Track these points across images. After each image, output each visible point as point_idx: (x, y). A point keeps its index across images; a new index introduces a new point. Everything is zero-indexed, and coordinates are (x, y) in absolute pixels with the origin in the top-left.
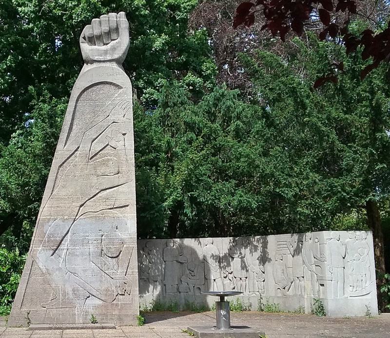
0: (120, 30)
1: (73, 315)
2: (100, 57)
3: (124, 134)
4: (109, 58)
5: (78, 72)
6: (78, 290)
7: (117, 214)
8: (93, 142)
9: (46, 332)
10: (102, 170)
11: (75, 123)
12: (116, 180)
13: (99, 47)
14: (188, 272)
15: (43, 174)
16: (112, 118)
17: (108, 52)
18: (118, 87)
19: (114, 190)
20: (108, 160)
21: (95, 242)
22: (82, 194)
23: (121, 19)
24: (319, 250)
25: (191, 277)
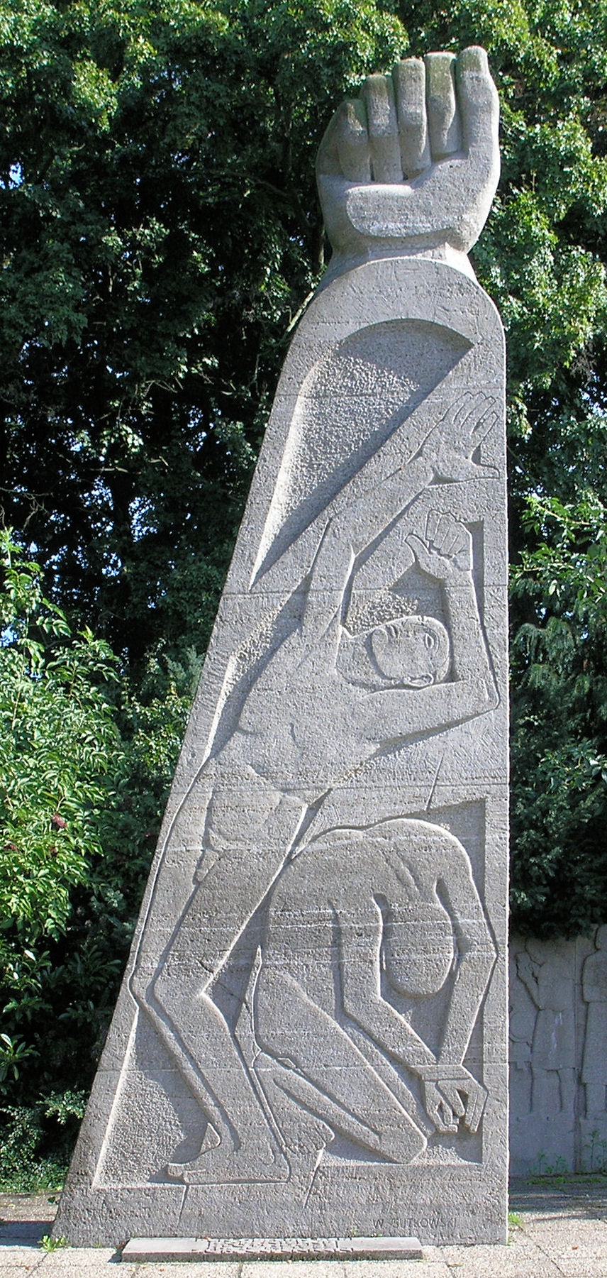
12: (433, 701)
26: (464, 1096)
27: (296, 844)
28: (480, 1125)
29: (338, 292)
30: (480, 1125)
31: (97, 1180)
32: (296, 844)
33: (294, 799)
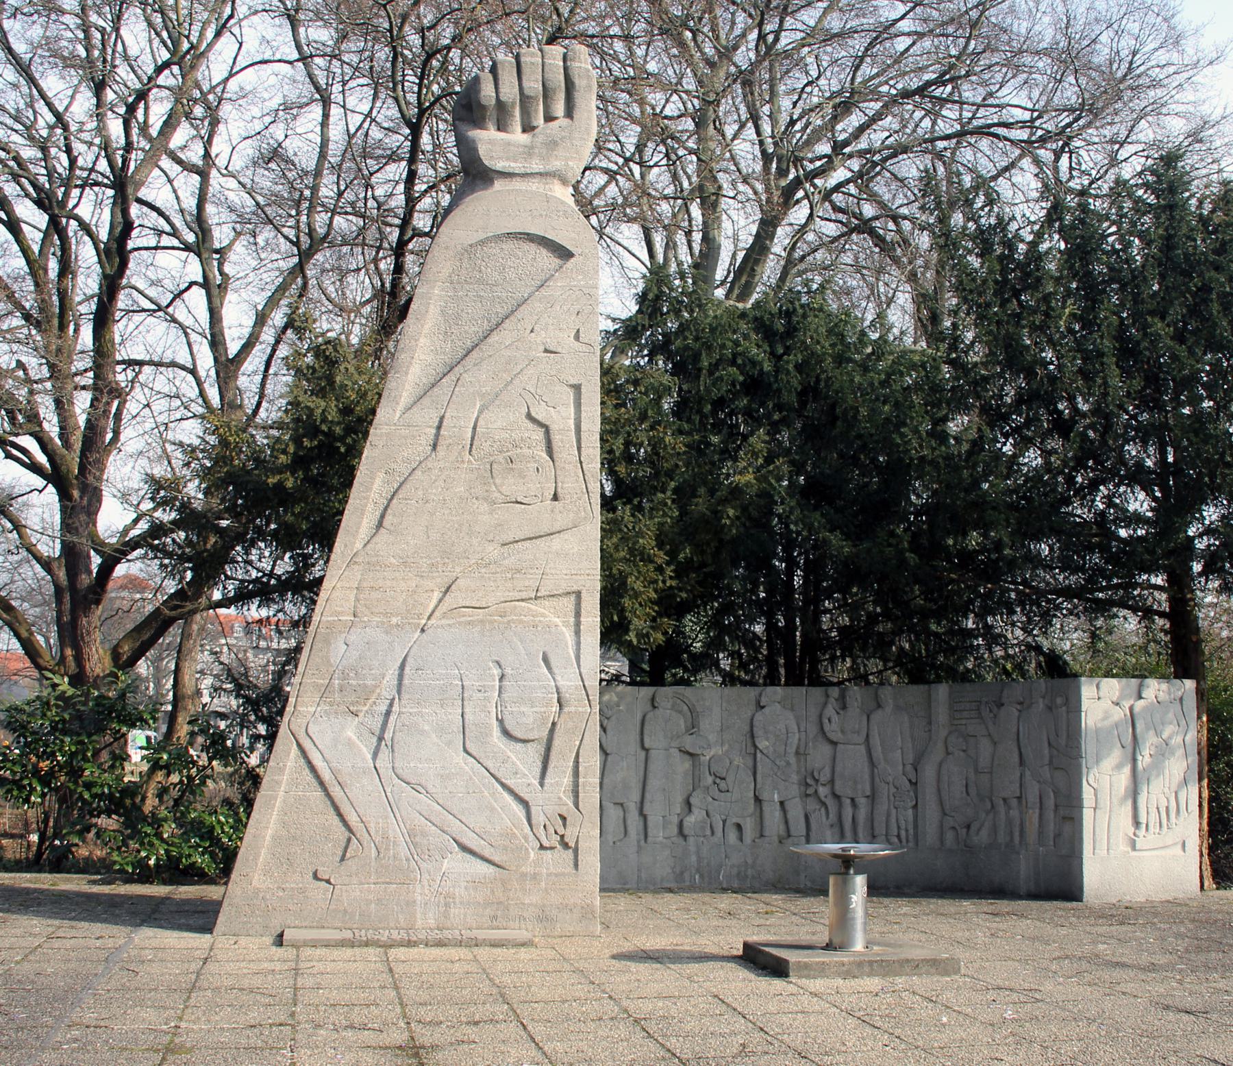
1: (407, 904)
2: (513, 164)
6: (424, 834)
7: (543, 615)
9: (336, 953)
10: (511, 486)
12: (543, 515)
14: (710, 780)
15: (615, 571)
17: (536, 151)
21: (479, 695)
24: (1064, 728)
25: (717, 794)
26: (564, 819)
27: (429, 618)
28: (577, 842)
29: (471, 209)
30: (577, 842)
31: (258, 880)
32: (429, 618)
33: (429, 584)
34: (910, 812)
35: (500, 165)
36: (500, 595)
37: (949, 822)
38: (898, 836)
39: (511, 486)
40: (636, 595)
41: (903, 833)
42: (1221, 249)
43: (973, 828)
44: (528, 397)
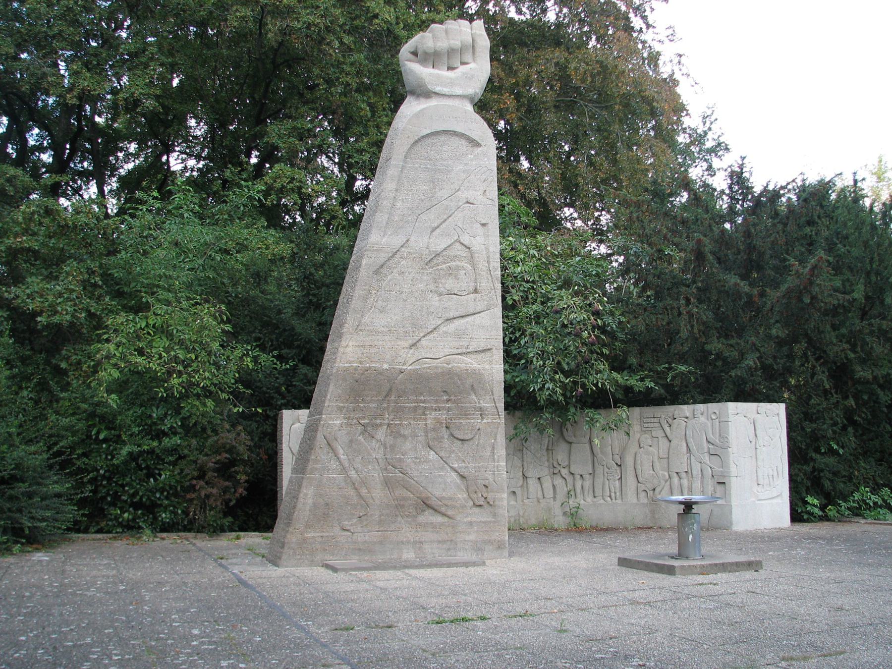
0: (477, 49)
3: (484, 225)
4: (459, 91)
5: (304, 328)
8: (432, 232)
10: (449, 284)
11: (429, 131)
12: (470, 302)
13: (439, 72)
16: (463, 195)
18: (475, 143)
19: (467, 323)
20: (458, 268)
22: (414, 325)
23: (475, 33)
34: (617, 483)
35: (438, 89)
36: (447, 351)
37: (642, 487)
38: (610, 496)
39: (449, 284)
40: (122, 324)
41: (613, 495)
42: (875, 297)
43: (657, 490)
44: (459, 230)
